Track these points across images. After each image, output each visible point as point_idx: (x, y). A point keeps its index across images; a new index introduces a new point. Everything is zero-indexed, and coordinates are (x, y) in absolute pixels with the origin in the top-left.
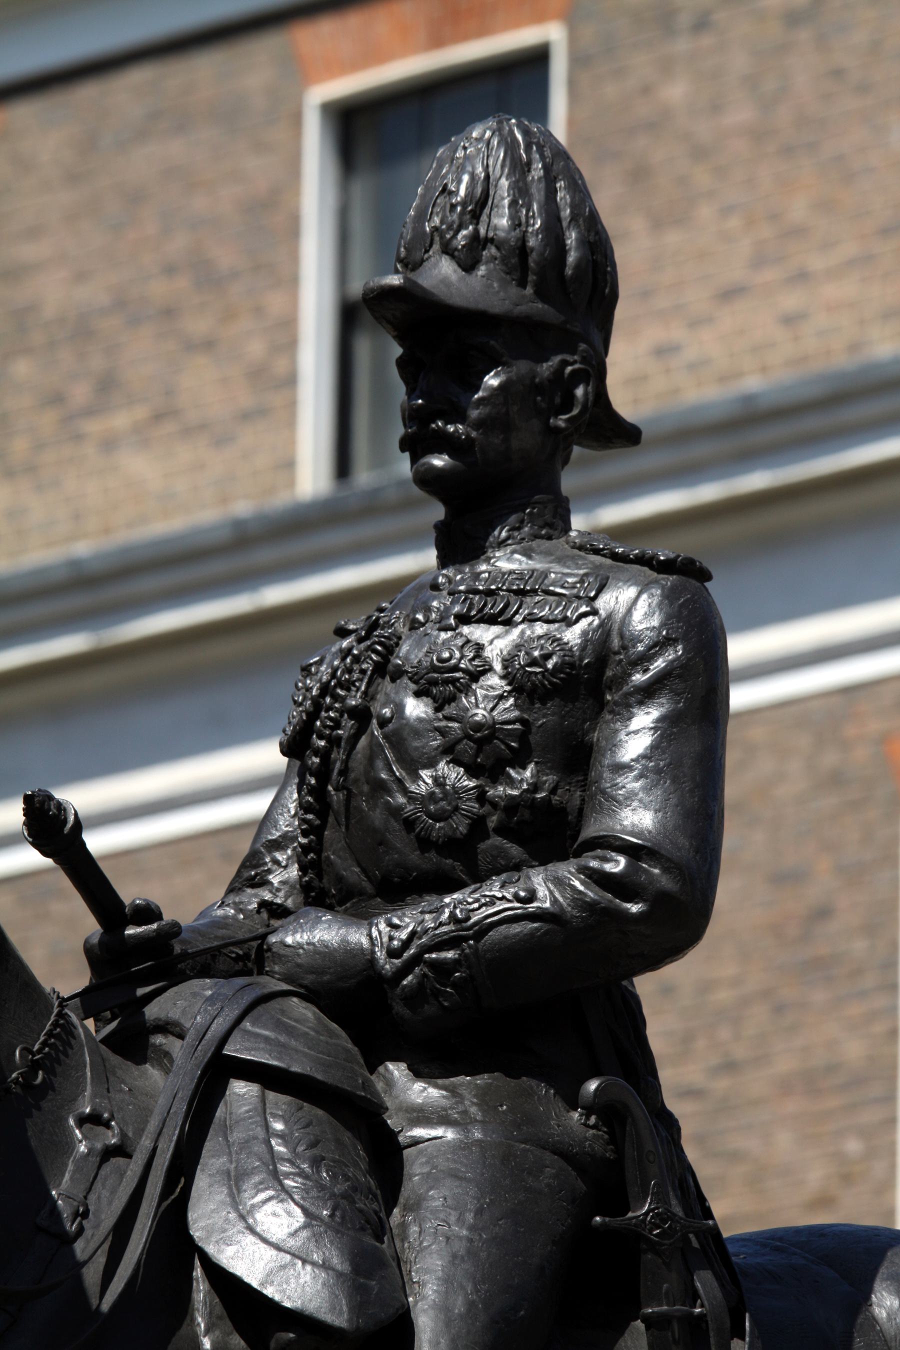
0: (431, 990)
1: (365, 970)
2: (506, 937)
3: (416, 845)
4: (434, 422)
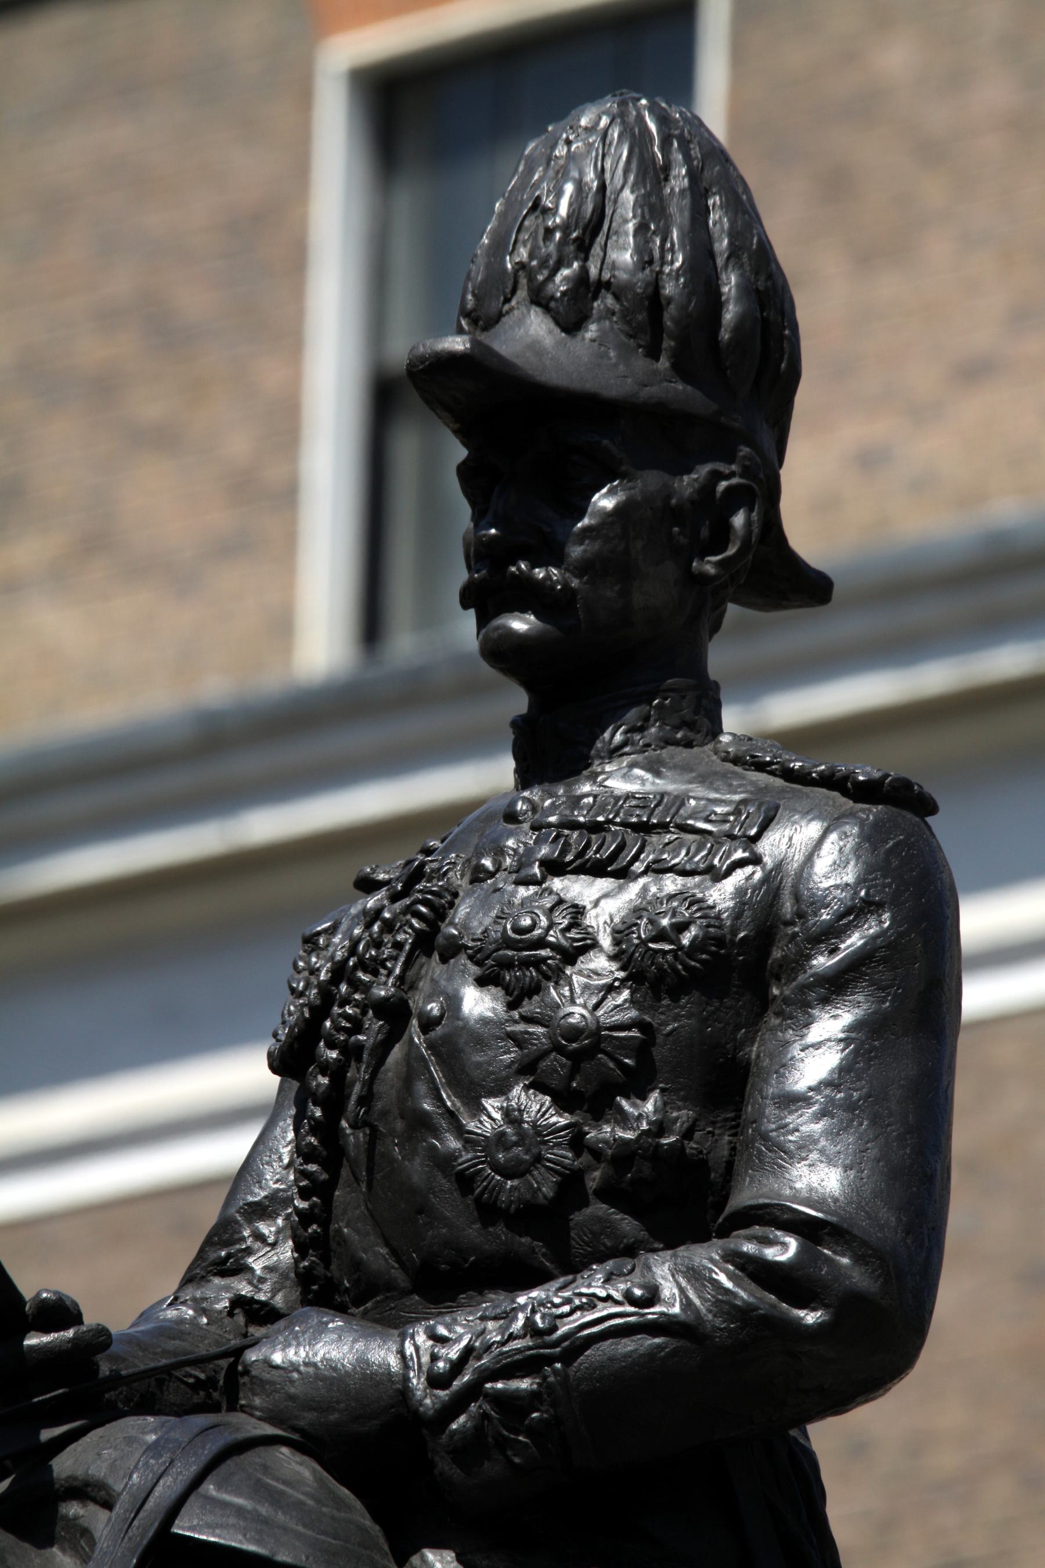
1: (392, 1407)
2: (611, 1359)
3: (475, 1214)
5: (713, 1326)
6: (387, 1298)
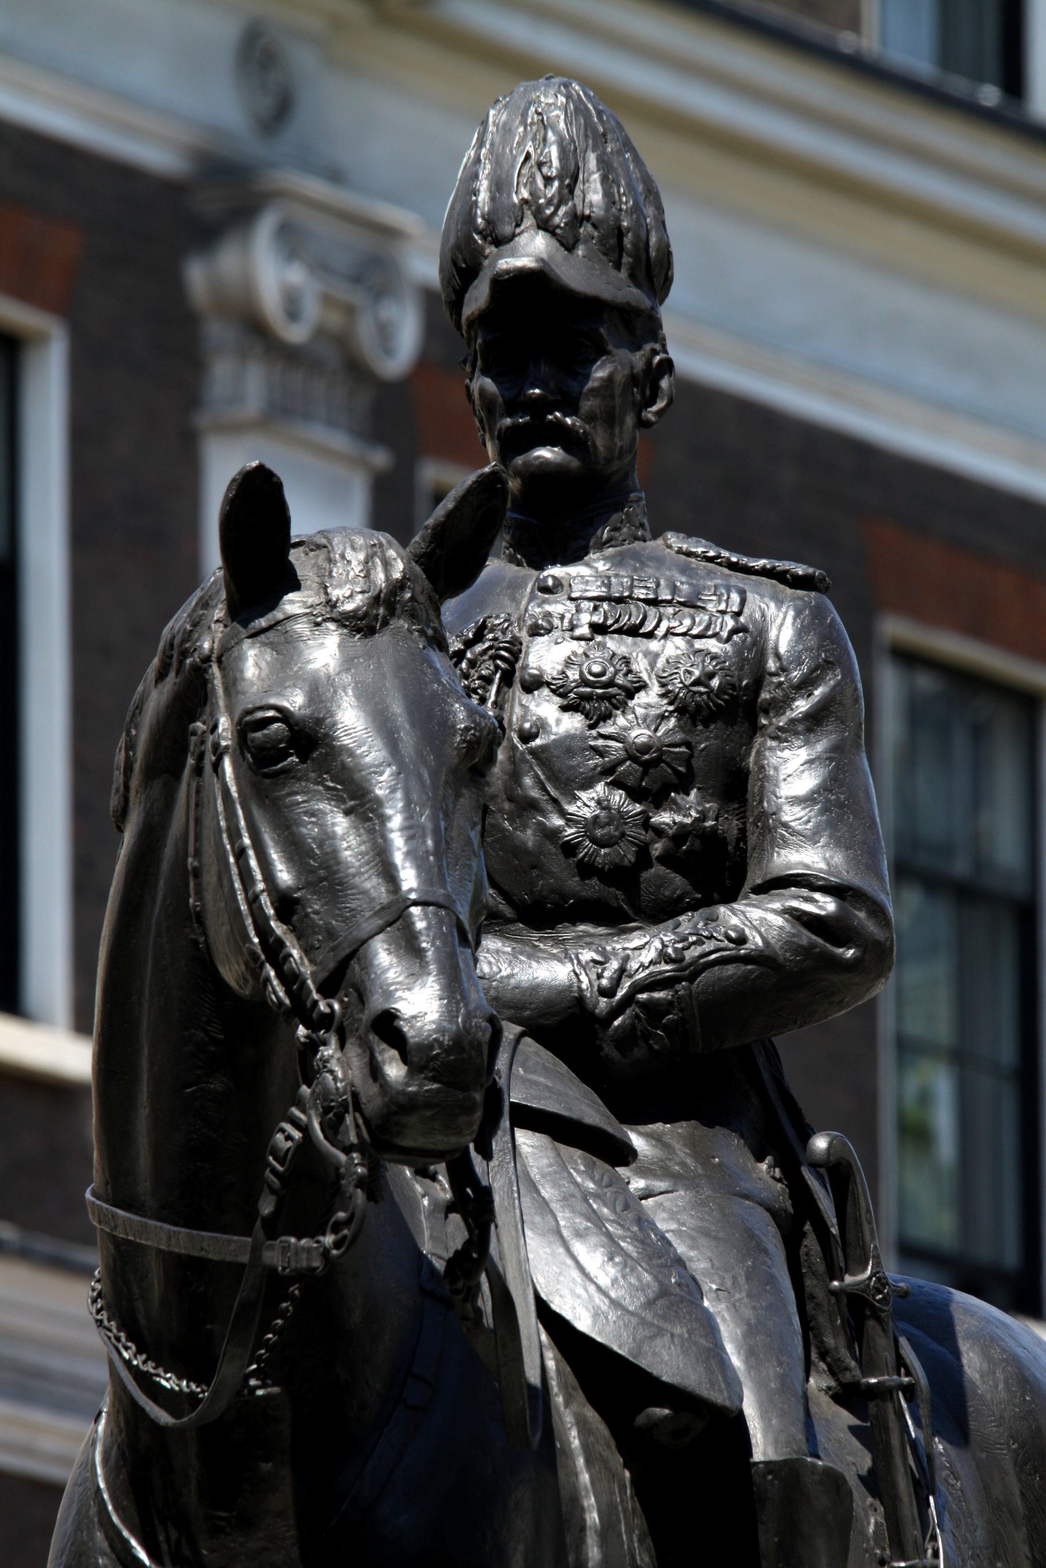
0: (641, 1031)
1: (570, 1008)
2: (720, 979)
3: (575, 870)
4: (551, 413)
5: (785, 959)
6: (492, 923)
